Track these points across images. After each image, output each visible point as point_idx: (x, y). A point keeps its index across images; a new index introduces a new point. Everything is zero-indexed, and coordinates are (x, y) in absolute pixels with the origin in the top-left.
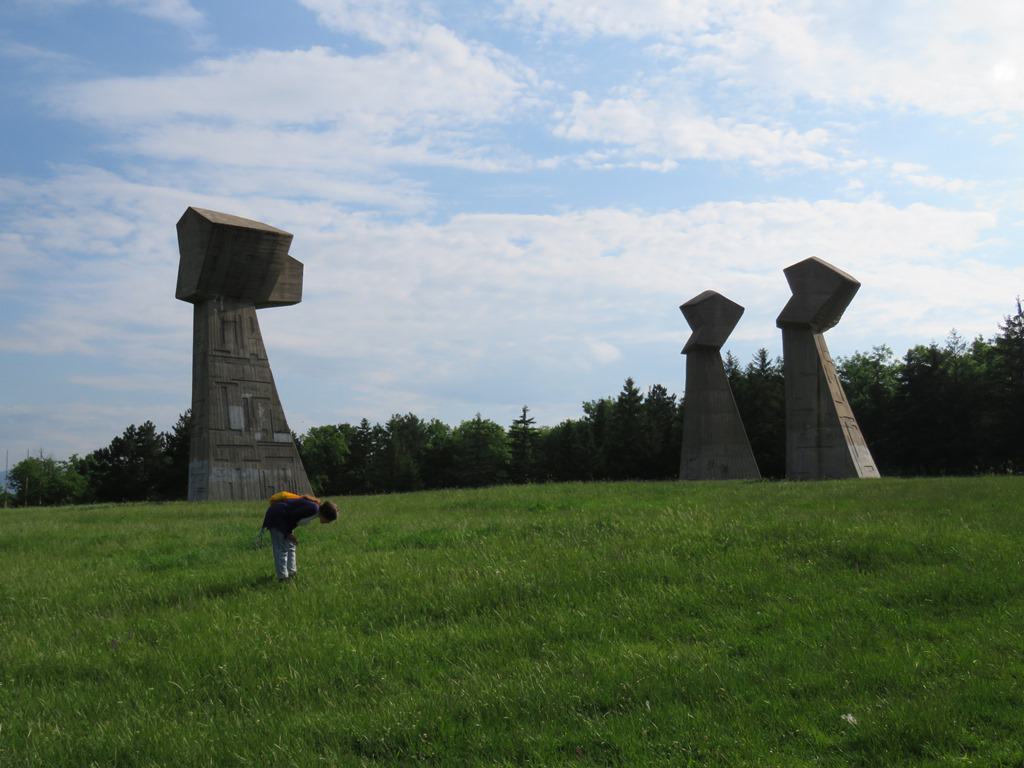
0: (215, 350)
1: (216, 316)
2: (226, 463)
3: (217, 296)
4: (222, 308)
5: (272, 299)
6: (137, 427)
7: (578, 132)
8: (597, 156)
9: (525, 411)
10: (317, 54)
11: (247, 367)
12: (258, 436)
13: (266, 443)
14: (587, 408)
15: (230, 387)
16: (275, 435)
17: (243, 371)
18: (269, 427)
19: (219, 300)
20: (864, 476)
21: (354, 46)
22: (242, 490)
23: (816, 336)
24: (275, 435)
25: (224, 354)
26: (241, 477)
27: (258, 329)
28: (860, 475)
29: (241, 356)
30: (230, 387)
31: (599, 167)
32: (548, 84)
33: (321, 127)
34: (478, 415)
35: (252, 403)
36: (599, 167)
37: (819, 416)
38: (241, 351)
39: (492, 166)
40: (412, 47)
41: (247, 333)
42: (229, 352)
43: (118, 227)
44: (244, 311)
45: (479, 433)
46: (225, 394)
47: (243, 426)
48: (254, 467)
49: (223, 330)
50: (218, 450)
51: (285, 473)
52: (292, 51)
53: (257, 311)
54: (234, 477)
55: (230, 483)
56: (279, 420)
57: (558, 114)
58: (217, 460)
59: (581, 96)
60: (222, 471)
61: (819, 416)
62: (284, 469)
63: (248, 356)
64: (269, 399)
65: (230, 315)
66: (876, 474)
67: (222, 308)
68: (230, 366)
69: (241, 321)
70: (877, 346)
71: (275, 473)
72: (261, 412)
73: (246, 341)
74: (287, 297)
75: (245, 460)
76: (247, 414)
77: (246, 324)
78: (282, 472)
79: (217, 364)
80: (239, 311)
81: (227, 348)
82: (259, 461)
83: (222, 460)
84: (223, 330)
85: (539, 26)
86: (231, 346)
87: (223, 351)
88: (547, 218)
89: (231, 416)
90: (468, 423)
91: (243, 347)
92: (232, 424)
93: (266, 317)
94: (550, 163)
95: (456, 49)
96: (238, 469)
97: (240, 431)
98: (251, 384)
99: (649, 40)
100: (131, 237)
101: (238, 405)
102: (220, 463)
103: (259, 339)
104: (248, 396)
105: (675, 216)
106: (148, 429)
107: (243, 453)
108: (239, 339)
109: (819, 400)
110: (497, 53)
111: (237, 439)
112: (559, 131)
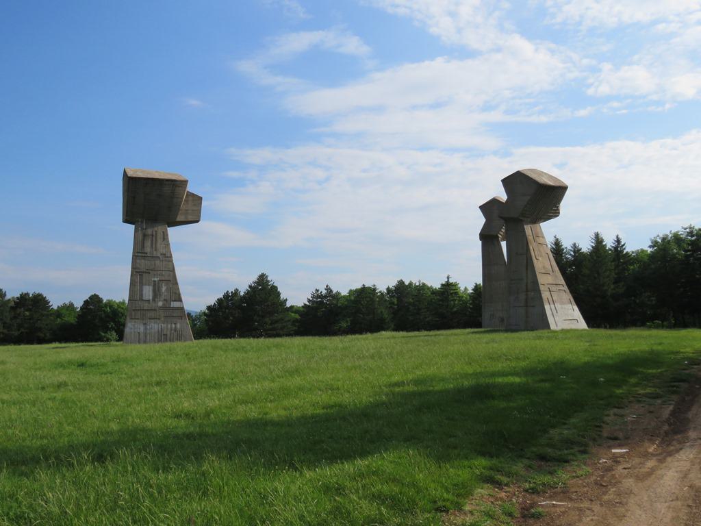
0: (138, 252)
1: (140, 232)
2: (137, 320)
3: (140, 220)
4: (144, 227)
5: (179, 219)
6: (230, 292)
7: (604, 89)
8: (615, 104)
9: (448, 278)
10: (439, 64)
11: (157, 262)
12: (160, 304)
13: (164, 308)
14: (328, 288)
15: (144, 275)
16: (172, 303)
17: (155, 265)
18: (168, 298)
19: (142, 222)
20: (559, 328)
21: (462, 53)
22: (146, 337)
23: (528, 229)
24: (172, 303)
25: (143, 255)
26: (146, 329)
27: (168, 238)
28: (553, 327)
29: (154, 255)
30: (144, 275)
31: (618, 112)
32: (585, 61)
33: (437, 105)
34: (364, 285)
35: (159, 283)
36: (618, 112)
37: (527, 286)
38: (155, 252)
39: (544, 119)
40: (499, 50)
41: (160, 241)
42: (146, 253)
43: (320, 174)
44: (159, 229)
45: (365, 294)
46: (141, 279)
47: (151, 298)
48: (155, 323)
49: (143, 240)
50: (133, 312)
51: (176, 327)
52: (423, 61)
53: (168, 229)
54: (142, 328)
55: (139, 333)
56: (175, 293)
57: (591, 81)
58: (132, 319)
59: (606, 66)
60: (134, 325)
61: (527, 286)
62: (175, 324)
63: (159, 255)
64: (170, 281)
65: (149, 231)
66: (582, 324)
67: (144, 227)
68: (146, 261)
69: (156, 234)
70: (685, 227)
71: (169, 326)
72: (164, 289)
73: (158, 245)
74: (190, 218)
75: (150, 319)
76: (154, 291)
77: (160, 235)
78: (174, 326)
79: (138, 261)
80: (156, 229)
81: (146, 251)
82: (159, 319)
83: (135, 319)
84: (143, 240)
85: (580, 23)
86: (148, 250)
87: (144, 253)
88: (579, 149)
89: (144, 292)
90: (356, 291)
91: (156, 250)
92: (144, 296)
93: (174, 233)
94: (583, 113)
95: (525, 47)
96: (145, 324)
97: (149, 301)
98: (159, 272)
99: (655, 23)
100: (327, 179)
101: (149, 285)
102: (133, 321)
103: (168, 245)
104: (156, 279)
105: (669, 141)
106: (72, 305)
107: (150, 314)
108: (154, 246)
109: (527, 273)
110: (552, 46)
111: (146, 306)
112: (591, 91)
